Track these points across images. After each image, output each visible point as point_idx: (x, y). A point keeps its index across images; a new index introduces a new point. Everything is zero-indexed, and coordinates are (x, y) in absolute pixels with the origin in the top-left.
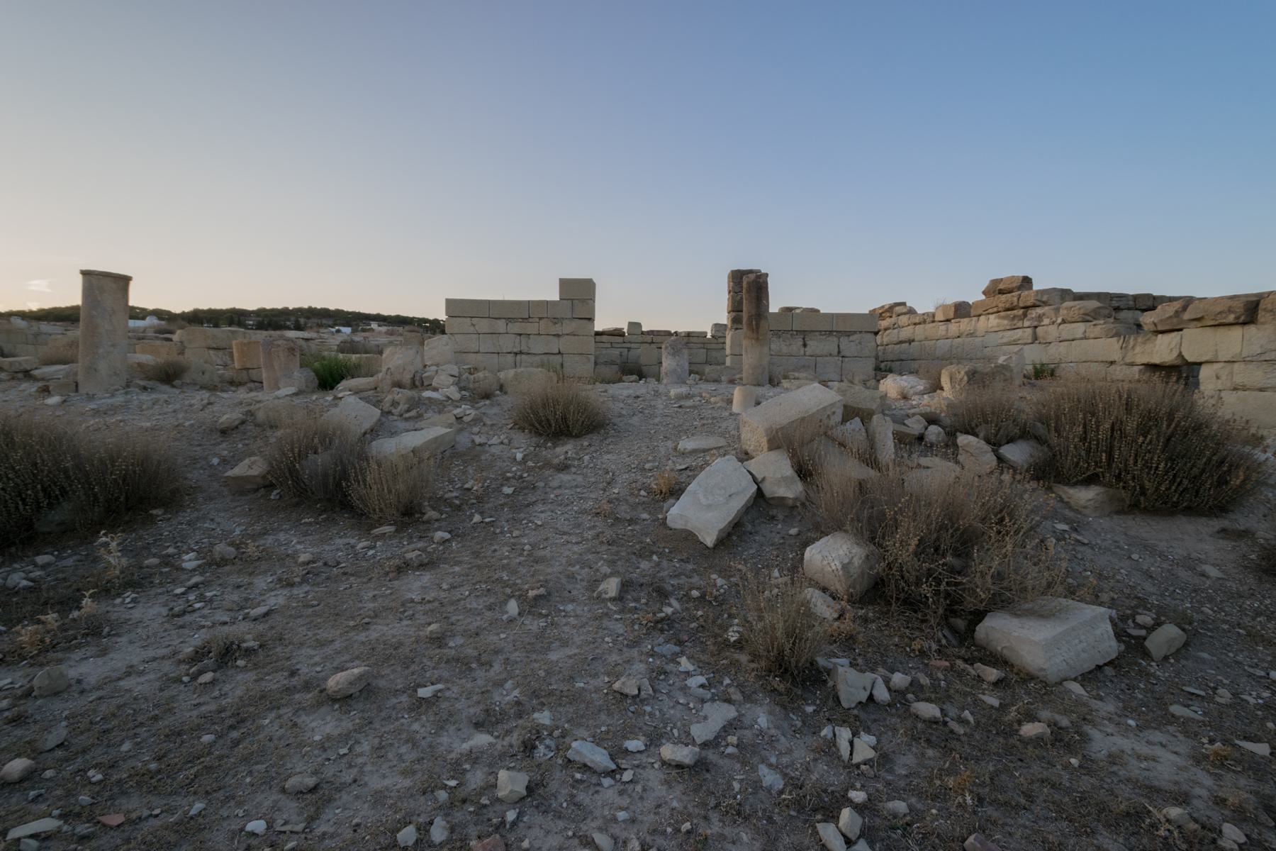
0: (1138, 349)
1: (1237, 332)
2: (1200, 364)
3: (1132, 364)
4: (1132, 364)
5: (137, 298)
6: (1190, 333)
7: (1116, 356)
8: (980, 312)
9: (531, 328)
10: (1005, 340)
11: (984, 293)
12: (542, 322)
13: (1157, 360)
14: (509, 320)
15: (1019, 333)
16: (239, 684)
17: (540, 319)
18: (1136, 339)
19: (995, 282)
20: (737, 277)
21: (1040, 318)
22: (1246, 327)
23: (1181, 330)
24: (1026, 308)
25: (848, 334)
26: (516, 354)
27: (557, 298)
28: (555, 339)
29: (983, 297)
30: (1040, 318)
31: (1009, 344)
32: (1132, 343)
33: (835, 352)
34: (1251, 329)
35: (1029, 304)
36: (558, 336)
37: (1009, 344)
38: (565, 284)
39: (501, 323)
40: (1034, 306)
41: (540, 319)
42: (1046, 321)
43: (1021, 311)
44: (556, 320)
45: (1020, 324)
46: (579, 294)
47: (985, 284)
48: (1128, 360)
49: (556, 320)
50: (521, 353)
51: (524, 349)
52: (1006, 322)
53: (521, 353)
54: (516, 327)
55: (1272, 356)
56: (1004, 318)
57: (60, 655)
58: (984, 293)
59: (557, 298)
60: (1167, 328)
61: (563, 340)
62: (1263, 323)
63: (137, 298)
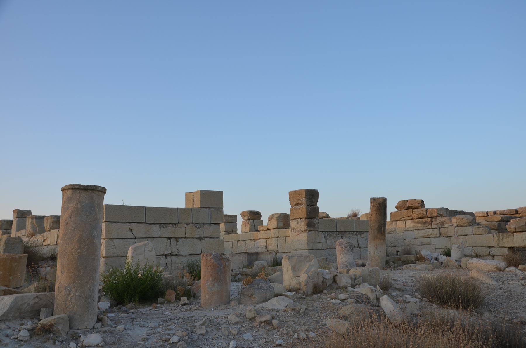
0: (505, 240)
3: (503, 247)
4: (503, 247)
5: (109, 199)
7: (494, 243)
8: (399, 219)
9: (179, 232)
10: (420, 235)
11: (397, 207)
12: (188, 227)
13: (517, 245)
14: (163, 225)
15: (430, 231)
18: (503, 235)
19: (404, 202)
21: (442, 223)
24: (432, 217)
25: (361, 233)
26: (166, 256)
28: (198, 241)
29: (396, 210)
30: (442, 223)
31: (424, 237)
32: (501, 237)
33: (356, 246)
35: (433, 215)
36: (200, 238)
37: (424, 237)
38: (294, 195)
39: (156, 228)
40: (437, 217)
41: (187, 224)
42: (446, 225)
43: (429, 219)
44: (199, 226)
45: (430, 226)
46: (85, 197)
47: (396, 204)
48: (501, 245)
49: (199, 226)
50: (171, 255)
51: (174, 251)
52: (420, 225)
53: (171, 255)
54: (167, 232)
56: (418, 223)
58: (397, 207)
61: (204, 241)
63: (109, 199)
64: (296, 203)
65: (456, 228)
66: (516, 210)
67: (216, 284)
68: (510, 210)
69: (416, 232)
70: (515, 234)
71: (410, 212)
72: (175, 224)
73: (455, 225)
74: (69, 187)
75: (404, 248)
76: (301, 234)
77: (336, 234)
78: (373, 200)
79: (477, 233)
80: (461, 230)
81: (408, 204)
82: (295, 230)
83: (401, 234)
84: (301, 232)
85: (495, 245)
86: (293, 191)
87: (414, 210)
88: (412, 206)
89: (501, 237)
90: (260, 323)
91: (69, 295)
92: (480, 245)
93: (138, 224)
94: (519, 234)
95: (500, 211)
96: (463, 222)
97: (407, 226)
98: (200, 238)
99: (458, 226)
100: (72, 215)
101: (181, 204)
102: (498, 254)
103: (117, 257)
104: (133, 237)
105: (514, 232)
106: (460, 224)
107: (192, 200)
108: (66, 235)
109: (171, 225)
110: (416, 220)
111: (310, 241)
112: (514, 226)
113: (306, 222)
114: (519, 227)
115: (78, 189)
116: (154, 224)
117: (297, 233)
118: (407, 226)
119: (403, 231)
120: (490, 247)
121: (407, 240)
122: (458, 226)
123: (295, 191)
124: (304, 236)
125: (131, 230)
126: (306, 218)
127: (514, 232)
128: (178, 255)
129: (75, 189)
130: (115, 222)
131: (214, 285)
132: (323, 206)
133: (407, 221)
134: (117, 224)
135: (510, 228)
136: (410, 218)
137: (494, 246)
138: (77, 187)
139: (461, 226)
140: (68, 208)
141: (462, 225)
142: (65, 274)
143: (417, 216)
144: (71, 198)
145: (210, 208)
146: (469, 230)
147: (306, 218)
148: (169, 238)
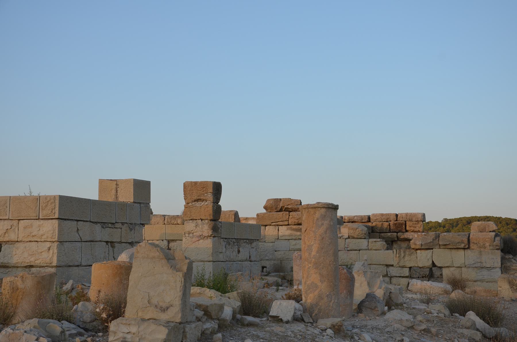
0: (407, 258)
1: (462, 252)
2: (442, 267)
3: (403, 267)
4: (403, 267)
5: (340, 213)
6: (436, 250)
16: (403, 333)
19: (277, 201)
20: (338, 206)
22: (466, 251)
23: (432, 249)
29: (264, 211)
32: (403, 255)
34: (468, 252)
41: (123, 224)
47: (264, 204)
48: (401, 264)
55: (2, 270)
57: (281, 334)
58: (265, 208)
60: (427, 247)
62: (473, 249)
64: (196, 198)
65: (347, 240)
66: (369, 218)
67: (349, 297)
68: (361, 216)
69: (293, 242)
70: (418, 251)
71: (286, 215)
72: (113, 224)
73: (346, 236)
74: (324, 206)
75: (276, 262)
76: (201, 241)
77: (234, 243)
78: (338, 206)
79: (374, 248)
80: (353, 243)
81: (281, 205)
82: (191, 235)
83: (271, 244)
84: (202, 237)
85: (395, 263)
86: (191, 182)
87: (291, 213)
88: (289, 207)
89: (403, 255)
90: (420, 331)
91: (331, 301)
92: (374, 263)
93: (85, 223)
94: (423, 251)
95: (349, 217)
96: (357, 233)
97: (280, 234)
99: (349, 238)
100: (326, 231)
101: (94, 195)
102: (397, 275)
103: (66, 266)
104: (80, 240)
105: (417, 250)
106: (353, 235)
107: (114, 192)
108: (322, 249)
109: (110, 225)
110: (295, 227)
111: (215, 251)
112: (420, 243)
113: (211, 226)
114: (426, 244)
115: (331, 208)
116: (96, 223)
117: (194, 239)
118: (280, 234)
119: (273, 241)
120: (387, 266)
121: (279, 253)
122: (349, 238)
123: (196, 183)
124: (208, 244)
126: (211, 220)
127: (417, 250)
129: (329, 208)
130: (65, 219)
131: (347, 298)
132: (226, 204)
133: (280, 227)
134: (68, 222)
135: (415, 244)
136: (286, 223)
137: (392, 266)
138: (330, 206)
139: (353, 238)
140: (322, 224)
141: (355, 236)
142: (326, 283)
143: (296, 221)
144: (325, 216)
145: (140, 203)
146: (364, 243)
147: (211, 220)
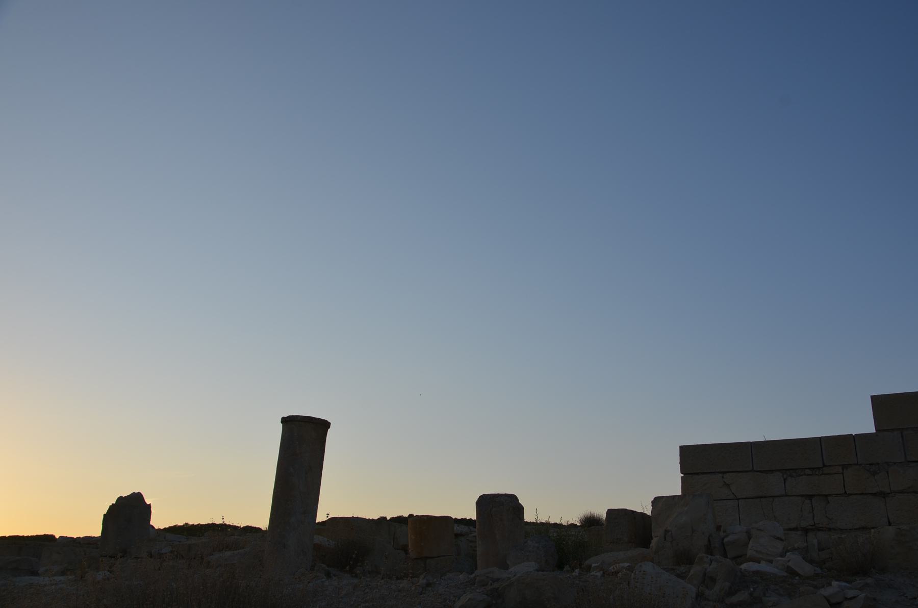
17: (844, 467)
26: (806, 531)
27: (871, 428)
36: (883, 495)
41: (844, 467)
59: (871, 428)
98: (883, 495)
116: (772, 471)
125: (727, 485)
128: (830, 529)
130: (698, 474)
148: (810, 497)
